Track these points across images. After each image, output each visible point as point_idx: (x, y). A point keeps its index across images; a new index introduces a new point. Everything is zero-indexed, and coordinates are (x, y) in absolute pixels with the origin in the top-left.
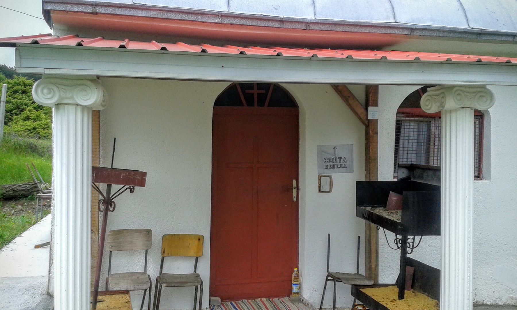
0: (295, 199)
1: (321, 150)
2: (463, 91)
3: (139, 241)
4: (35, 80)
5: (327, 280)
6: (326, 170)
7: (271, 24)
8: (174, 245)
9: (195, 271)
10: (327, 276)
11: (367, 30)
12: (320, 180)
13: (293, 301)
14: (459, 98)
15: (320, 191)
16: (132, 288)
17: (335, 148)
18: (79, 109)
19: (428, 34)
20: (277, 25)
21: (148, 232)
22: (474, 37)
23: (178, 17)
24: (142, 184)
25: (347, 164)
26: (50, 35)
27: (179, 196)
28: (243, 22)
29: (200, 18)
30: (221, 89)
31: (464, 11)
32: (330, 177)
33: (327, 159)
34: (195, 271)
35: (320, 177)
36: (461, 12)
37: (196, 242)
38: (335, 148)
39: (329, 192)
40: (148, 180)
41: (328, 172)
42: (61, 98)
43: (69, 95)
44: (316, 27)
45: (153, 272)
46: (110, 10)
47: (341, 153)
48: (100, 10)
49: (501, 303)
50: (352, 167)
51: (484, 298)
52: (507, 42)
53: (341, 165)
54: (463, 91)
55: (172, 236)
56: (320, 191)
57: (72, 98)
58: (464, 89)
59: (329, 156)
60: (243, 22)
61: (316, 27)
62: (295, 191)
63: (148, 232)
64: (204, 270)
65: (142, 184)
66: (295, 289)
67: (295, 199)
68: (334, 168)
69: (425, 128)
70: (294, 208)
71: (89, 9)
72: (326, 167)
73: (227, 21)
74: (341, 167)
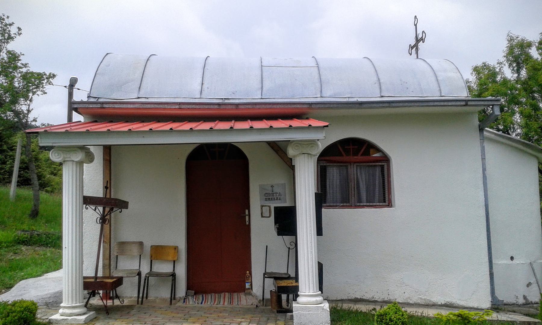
0: (247, 223)
1: (262, 188)
2: (300, 144)
3: (135, 250)
4: (50, 150)
5: (264, 277)
6: (266, 202)
7: (212, 107)
8: (158, 252)
9: (174, 270)
10: (264, 274)
11: (278, 106)
12: (262, 209)
13: (246, 295)
14: (296, 148)
15: (262, 217)
16: (125, 276)
17: (272, 186)
18: (74, 163)
19: (323, 106)
20: (216, 107)
21: (141, 244)
22: (358, 106)
23: (152, 106)
24: (127, 207)
25: (282, 197)
26: (80, 121)
27: (161, 218)
28: (194, 106)
29: (166, 106)
30: (194, 146)
31: (380, 83)
32: (269, 206)
33: (267, 194)
34: (174, 270)
35: (262, 206)
36: (377, 85)
37: (173, 251)
38: (272, 186)
39: (269, 217)
40: (130, 206)
41: (267, 203)
42: (64, 158)
43: (68, 156)
44: (242, 107)
45: (145, 270)
46: (111, 106)
47: (276, 190)
48: (105, 106)
49: (411, 302)
50: (286, 199)
51: (396, 297)
52: (387, 107)
53: (277, 198)
54: (300, 144)
55: (157, 246)
56: (262, 217)
57: (70, 158)
58: (300, 142)
59: (268, 192)
60: (194, 106)
61: (242, 107)
62: (247, 218)
63: (141, 244)
64: (181, 271)
65: (127, 207)
66: (247, 286)
67: (247, 223)
68: (272, 200)
69: (378, 171)
70: (247, 229)
71: (99, 106)
72: (266, 200)
73: (183, 107)
74: (277, 199)
